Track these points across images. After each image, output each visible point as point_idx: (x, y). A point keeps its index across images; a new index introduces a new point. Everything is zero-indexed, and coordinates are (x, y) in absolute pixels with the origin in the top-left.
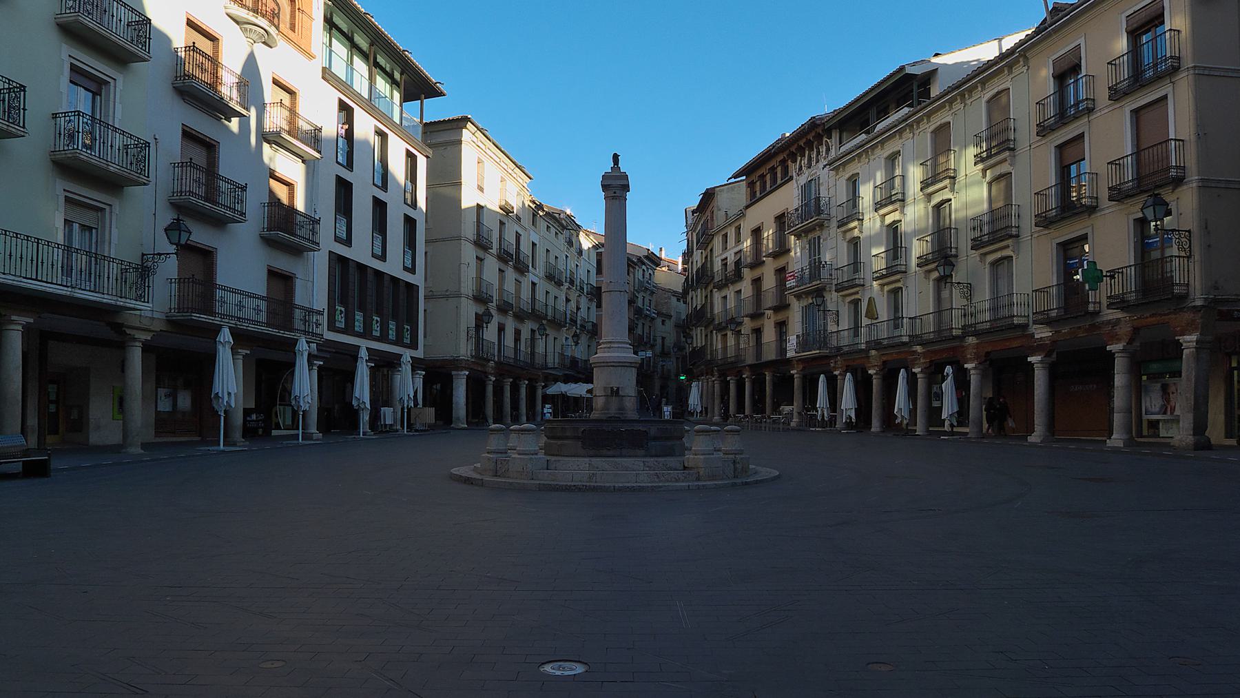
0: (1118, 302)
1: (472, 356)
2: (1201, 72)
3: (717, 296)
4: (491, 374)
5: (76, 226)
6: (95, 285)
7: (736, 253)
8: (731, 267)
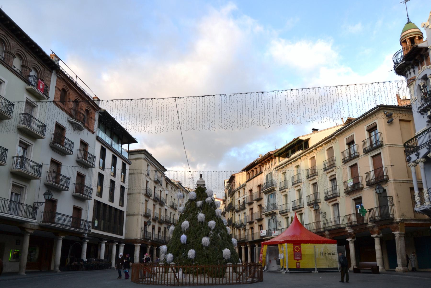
1: (143, 238)
2: (390, 146)
4: (149, 245)
5: (14, 194)
6: (17, 213)
7: (243, 199)
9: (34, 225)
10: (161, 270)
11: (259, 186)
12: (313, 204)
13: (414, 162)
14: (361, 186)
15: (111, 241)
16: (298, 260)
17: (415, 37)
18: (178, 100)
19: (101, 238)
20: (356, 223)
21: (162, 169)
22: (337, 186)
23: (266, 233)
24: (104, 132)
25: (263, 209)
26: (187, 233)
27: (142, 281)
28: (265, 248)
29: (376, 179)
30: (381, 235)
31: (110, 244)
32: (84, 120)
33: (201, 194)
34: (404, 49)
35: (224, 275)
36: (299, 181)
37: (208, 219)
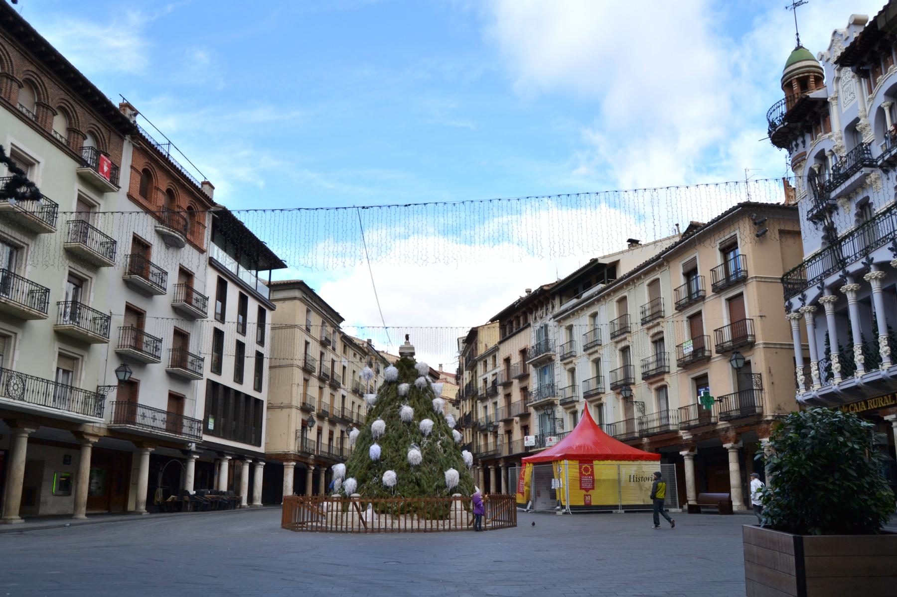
0: (725, 416)
1: (299, 452)
2: (760, 280)
3: (480, 406)
4: (311, 464)
5: (61, 371)
7: (493, 375)
8: (489, 385)
9: (100, 428)
10: (335, 508)
11: (523, 352)
12: (621, 386)
13: (797, 311)
14: (707, 354)
15: (239, 456)
16: (587, 490)
17: (808, 77)
18: (363, 212)
19: (220, 452)
20: (697, 422)
21: (333, 318)
22: (664, 352)
23: (536, 442)
24: (222, 249)
25: (530, 395)
26: (381, 440)
27: (302, 527)
28: (529, 469)
29: (733, 340)
30: (741, 444)
31: (238, 463)
32: (185, 226)
33: (407, 371)
34: (788, 100)
35: (446, 516)
36: (571, 355)
37: (420, 416)
